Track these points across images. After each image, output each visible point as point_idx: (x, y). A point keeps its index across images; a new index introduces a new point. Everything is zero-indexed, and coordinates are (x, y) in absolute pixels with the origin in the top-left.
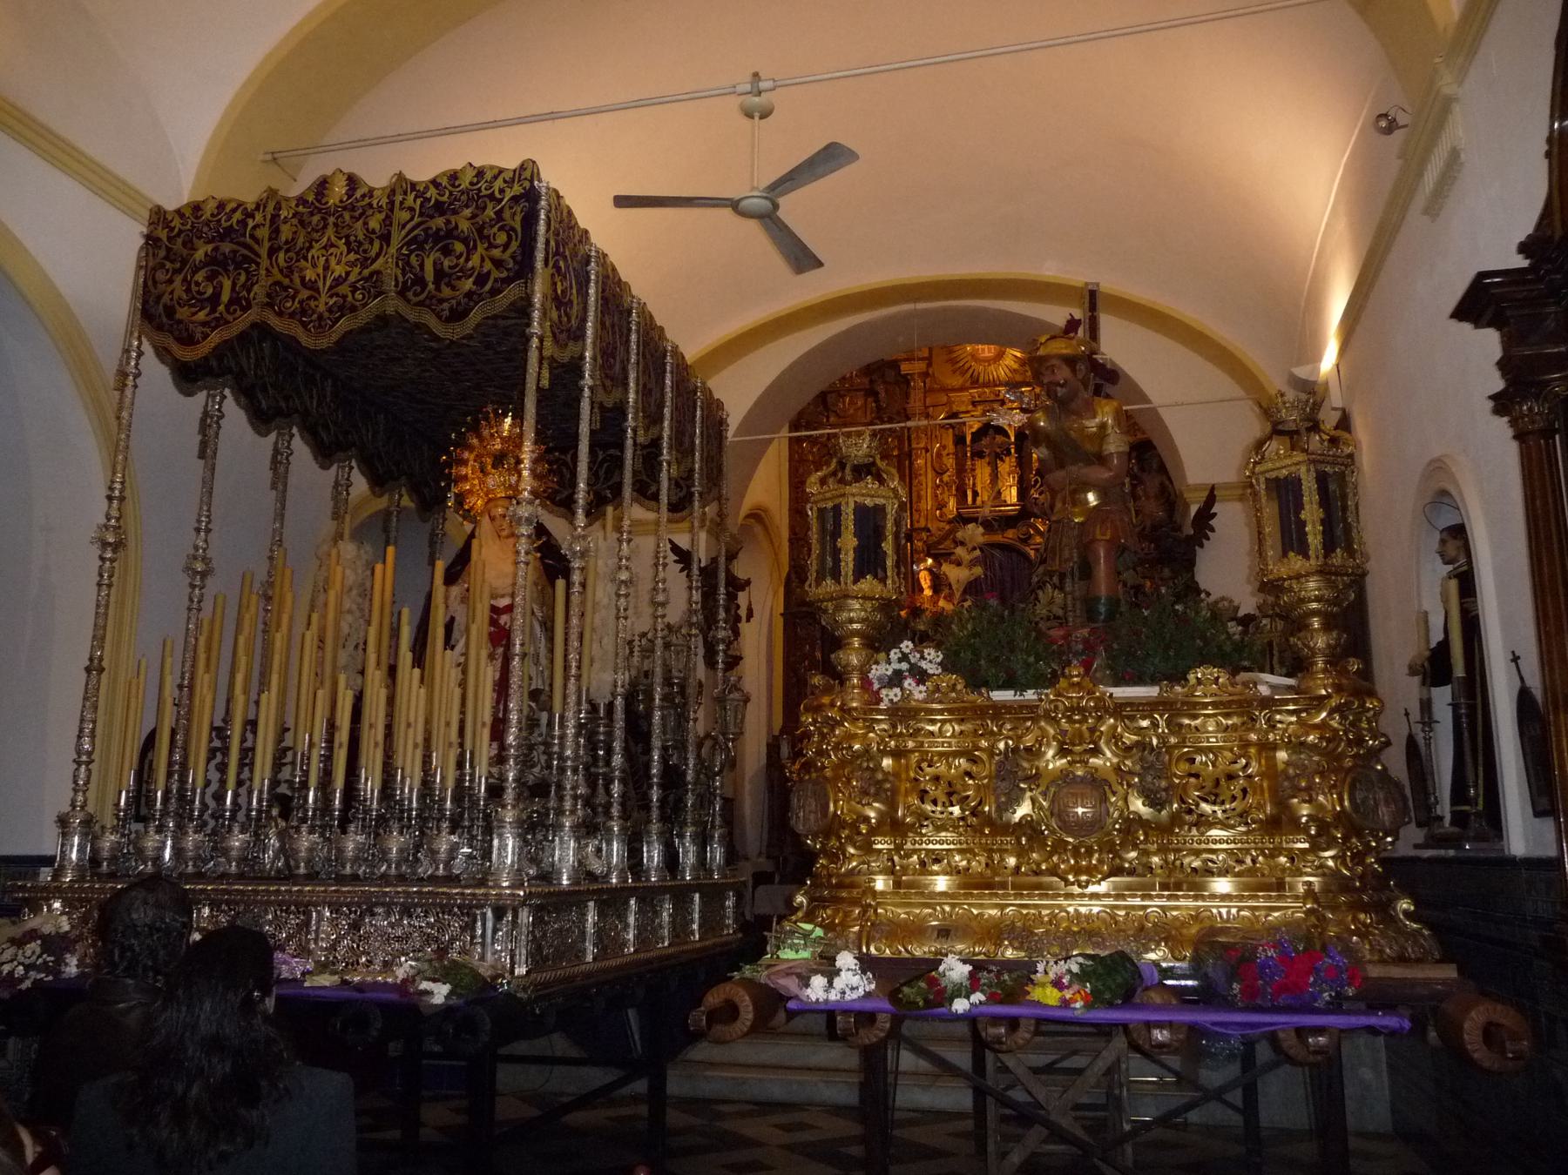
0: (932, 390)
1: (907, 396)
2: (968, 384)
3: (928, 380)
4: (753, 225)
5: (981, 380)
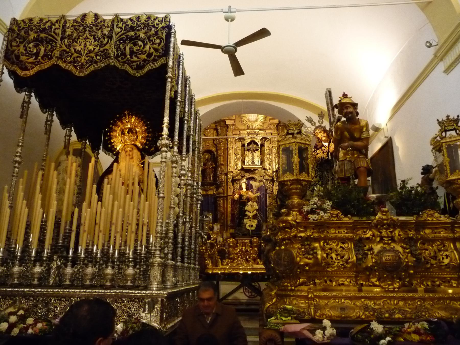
0: (235, 130)
1: (227, 131)
2: (246, 128)
3: (234, 126)
4: (226, 56)
5: (250, 128)
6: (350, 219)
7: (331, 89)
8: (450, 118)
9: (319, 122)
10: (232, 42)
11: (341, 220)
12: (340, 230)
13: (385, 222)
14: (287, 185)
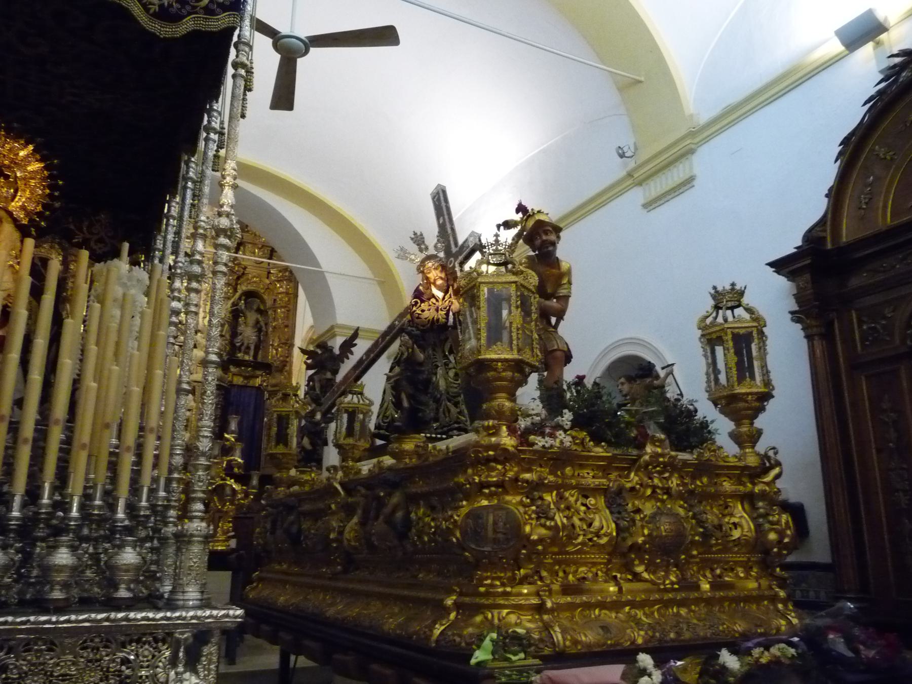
6: (605, 450)
8: (736, 287)
9: (435, 247)
10: (304, 32)
11: (589, 451)
12: (580, 471)
13: (661, 459)
14: (495, 370)
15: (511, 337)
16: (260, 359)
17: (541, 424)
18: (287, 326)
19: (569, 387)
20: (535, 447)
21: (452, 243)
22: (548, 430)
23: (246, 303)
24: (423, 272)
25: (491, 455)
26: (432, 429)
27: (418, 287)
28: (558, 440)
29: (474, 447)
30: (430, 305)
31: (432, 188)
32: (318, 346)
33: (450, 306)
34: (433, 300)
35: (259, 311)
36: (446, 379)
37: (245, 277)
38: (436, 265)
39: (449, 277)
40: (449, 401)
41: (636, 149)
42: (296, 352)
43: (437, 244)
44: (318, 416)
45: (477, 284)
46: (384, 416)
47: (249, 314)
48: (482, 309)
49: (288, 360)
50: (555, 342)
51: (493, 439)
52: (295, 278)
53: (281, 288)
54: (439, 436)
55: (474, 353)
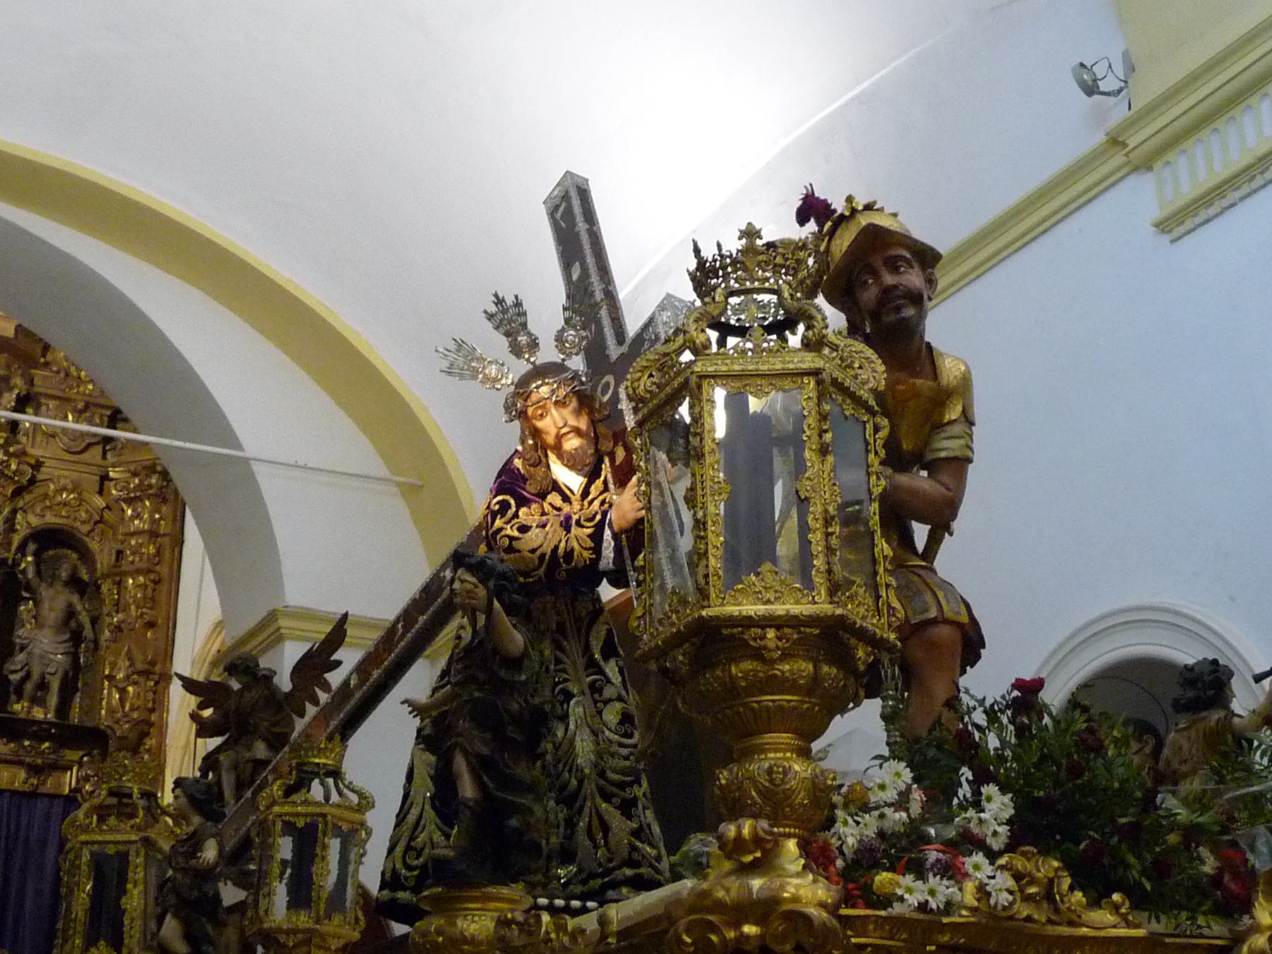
6: (1124, 917)
7: (587, 180)
9: (560, 339)
11: (1071, 923)
14: (758, 654)
15: (805, 544)
16: (75, 716)
17: (907, 834)
18: (151, 625)
19: (991, 714)
20: (897, 909)
21: (609, 332)
22: (933, 855)
23: (38, 563)
24: (522, 415)
25: (748, 937)
26: (554, 884)
27: (510, 461)
28: (970, 886)
29: (692, 910)
30: (543, 514)
31: (548, 184)
32: (231, 669)
33: (604, 514)
34: (554, 498)
35: (75, 583)
36: (594, 733)
37: (38, 491)
38: (562, 392)
39: (602, 429)
40: (607, 798)
41: (1130, 68)
42: (180, 703)
43: (563, 330)
44: (210, 853)
45: (694, 379)
46: (408, 848)
47: (45, 592)
48: (709, 459)
49: (153, 718)
50: (929, 597)
51: (756, 883)
52: (176, 492)
53: (138, 518)
54: (576, 904)
55: (684, 602)
